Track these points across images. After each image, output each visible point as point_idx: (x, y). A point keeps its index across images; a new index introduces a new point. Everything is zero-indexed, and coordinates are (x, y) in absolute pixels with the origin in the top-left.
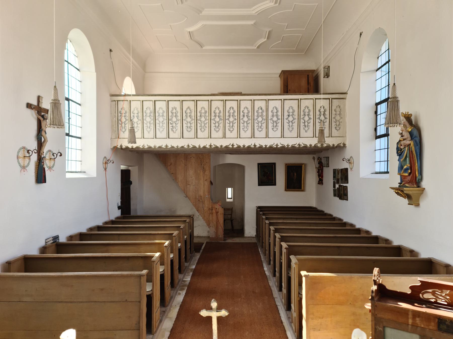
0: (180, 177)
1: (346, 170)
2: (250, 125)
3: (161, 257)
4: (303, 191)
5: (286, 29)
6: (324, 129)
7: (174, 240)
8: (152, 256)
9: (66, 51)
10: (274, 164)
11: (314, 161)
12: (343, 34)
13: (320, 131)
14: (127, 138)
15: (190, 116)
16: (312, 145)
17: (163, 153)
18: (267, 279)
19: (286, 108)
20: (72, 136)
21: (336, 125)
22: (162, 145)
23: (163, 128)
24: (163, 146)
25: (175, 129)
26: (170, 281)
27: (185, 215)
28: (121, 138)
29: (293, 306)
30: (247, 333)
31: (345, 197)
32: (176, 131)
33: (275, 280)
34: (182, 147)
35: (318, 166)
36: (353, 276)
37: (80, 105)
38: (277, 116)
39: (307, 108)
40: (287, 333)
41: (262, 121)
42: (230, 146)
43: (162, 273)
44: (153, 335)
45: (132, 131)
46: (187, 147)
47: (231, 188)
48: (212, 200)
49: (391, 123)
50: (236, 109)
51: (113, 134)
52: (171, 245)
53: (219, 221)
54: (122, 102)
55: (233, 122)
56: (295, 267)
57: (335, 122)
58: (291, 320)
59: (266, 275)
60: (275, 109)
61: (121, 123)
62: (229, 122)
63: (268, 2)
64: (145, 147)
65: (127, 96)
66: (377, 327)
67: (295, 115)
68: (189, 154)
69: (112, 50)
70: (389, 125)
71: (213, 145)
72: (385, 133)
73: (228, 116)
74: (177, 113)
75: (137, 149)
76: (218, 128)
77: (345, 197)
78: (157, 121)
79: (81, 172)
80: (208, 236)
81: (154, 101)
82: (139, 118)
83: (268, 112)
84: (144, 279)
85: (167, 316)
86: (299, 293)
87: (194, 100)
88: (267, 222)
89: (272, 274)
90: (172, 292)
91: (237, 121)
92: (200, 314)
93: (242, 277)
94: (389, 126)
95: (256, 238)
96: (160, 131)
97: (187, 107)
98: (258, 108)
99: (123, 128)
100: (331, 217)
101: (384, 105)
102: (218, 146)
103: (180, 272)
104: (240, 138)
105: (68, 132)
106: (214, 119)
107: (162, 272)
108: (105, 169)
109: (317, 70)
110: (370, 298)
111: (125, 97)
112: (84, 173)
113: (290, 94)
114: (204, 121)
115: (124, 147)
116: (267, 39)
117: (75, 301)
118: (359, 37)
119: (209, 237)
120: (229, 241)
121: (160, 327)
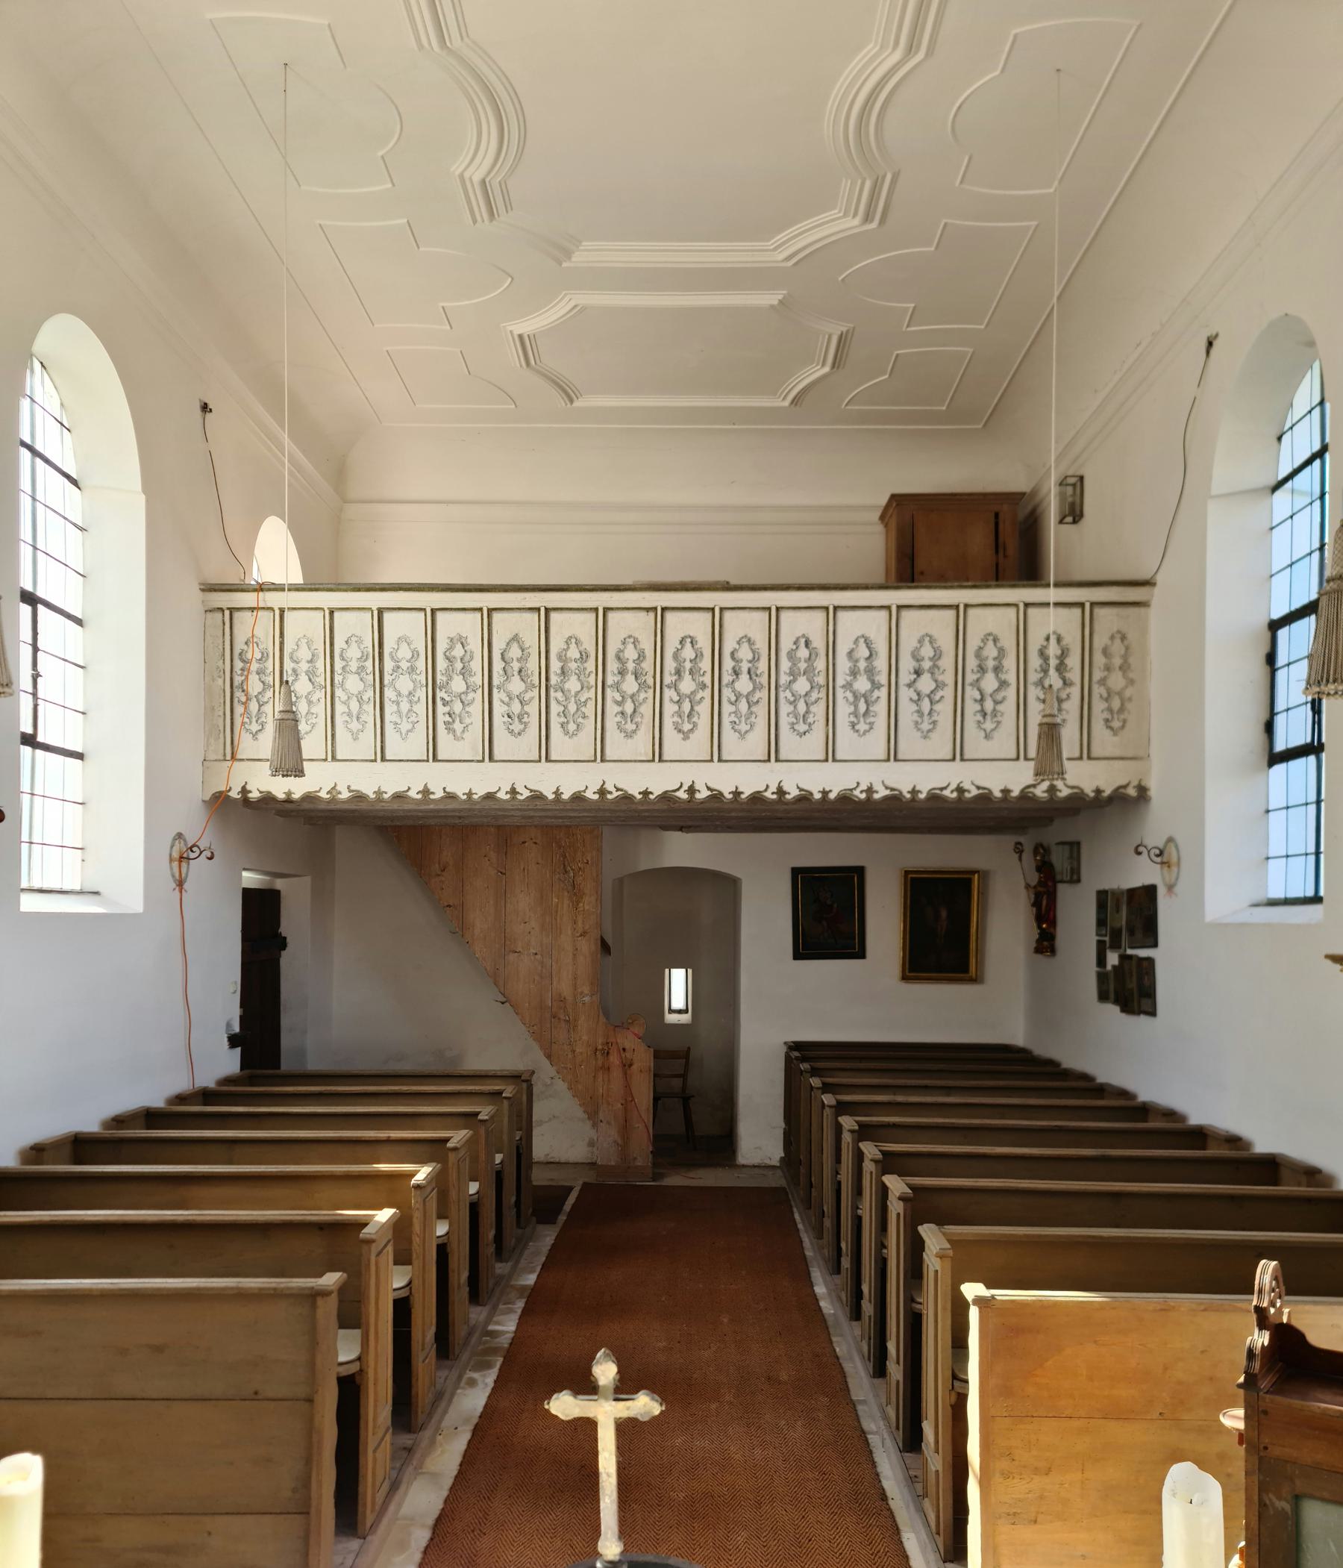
0: (480, 921)
1: (1150, 891)
2: (761, 710)
3: (400, 1228)
4: (976, 980)
5: (908, 326)
6: (1058, 720)
7: (450, 1164)
8: (364, 1222)
9: (25, 404)
10: (860, 871)
11: (1020, 859)
12: (1138, 346)
13: (1045, 728)
14: (268, 760)
15: (523, 674)
16: (1012, 791)
17: (410, 822)
18: (827, 1328)
19: (908, 643)
20: (47, 748)
21: (1110, 710)
22: (409, 788)
23: (413, 719)
24: (409, 793)
25: (461, 723)
26: (433, 1329)
27: (499, 1073)
28: (243, 760)
29: (928, 1428)
30: (741, 1537)
31: (1145, 1003)
32: (463, 731)
33: (858, 1332)
34: (490, 796)
35: (1034, 878)
36: (1172, 1304)
37: (79, 622)
38: (870, 672)
39: (990, 643)
40: (904, 1540)
41: (810, 691)
42: (682, 795)
43: (403, 1295)
44: (362, 1540)
45: (289, 725)
46: (508, 796)
47: (684, 970)
48: (606, 1014)
49: (1331, 680)
50: (704, 643)
51: (212, 741)
52: (438, 1181)
53: (633, 1100)
54: (248, 614)
55: (692, 697)
56: (938, 1269)
57: (1106, 700)
58: (919, 1487)
59: (823, 1315)
60: (864, 645)
61: (243, 699)
62: (676, 698)
63: (834, 213)
64: (340, 796)
65: (269, 590)
66: (1270, 1500)
67: (941, 671)
68: (518, 827)
69: (210, 406)
70: (1322, 687)
71: (613, 790)
72: (1309, 740)
73: (673, 672)
74: (467, 658)
75: (306, 806)
76: (632, 721)
77: (1145, 1003)
78: (389, 693)
79: (81, 893)
80: (589, 1161)
81: (376, 613)
82: (318, 680)
83: (834, 658)
84: (328, 1309)
85: (421, 1468)
86: (955, 1377)
87: (538, 609)
88: (828, 1099)
89: (848, 1309)
90: (442, 1374)
91: (708, 691)
92: (548, 1411)
93: (726, 1320)
94: (1324, 693)
95: (783, 1171)
96: (399, 731)
97: (509, 636)
98: (794, 639)
99: (254, 720)
100: (1086, 1086)
101: (1307, 626)
102: (630, 792)
103: (475, 1296)
104: (720, 760)
105: (29, 730)
106: (617, 686)
107: (400, 1292)
108: (181, 884)
109: (1034, 492)
110: (1242, 1379)
111: (261, 594)
112: (96, 897)
113: (924, 584)
114: (577, 693)
115: (254, 795)
116: (833, 366)
117: (50, 1394)
118: (1205, 355)
119: (592, 1165)
120: (675, 1180)
121: (392, 1508)
